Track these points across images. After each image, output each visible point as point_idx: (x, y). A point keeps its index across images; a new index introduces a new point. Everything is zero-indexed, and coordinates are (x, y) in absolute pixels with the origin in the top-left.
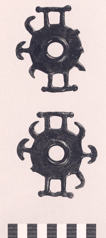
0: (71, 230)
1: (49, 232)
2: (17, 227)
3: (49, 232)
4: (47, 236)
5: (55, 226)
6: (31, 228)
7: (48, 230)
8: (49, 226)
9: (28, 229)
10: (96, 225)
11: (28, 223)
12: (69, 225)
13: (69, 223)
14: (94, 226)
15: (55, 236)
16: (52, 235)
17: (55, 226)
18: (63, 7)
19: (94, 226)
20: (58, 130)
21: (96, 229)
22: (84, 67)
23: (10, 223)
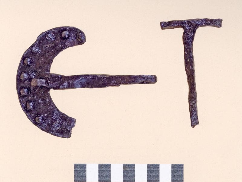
0: (177, 172)
2: (110, 167)
4: (147, 179)
5: (108, 166)
6: (103, 169)
7: (100, 171)
8: (101, 166)
9: (99, 171)
10: (183, 165)
11: (99, 163)
12: (77, 165)
13: (102, 163)
15: (157, 179)
16: (80, 177)
17: (108, 166)
18: (181, 28)
20: (50, 63)
21: (86, 170)
22: (73, 27)
23: (77, 163)
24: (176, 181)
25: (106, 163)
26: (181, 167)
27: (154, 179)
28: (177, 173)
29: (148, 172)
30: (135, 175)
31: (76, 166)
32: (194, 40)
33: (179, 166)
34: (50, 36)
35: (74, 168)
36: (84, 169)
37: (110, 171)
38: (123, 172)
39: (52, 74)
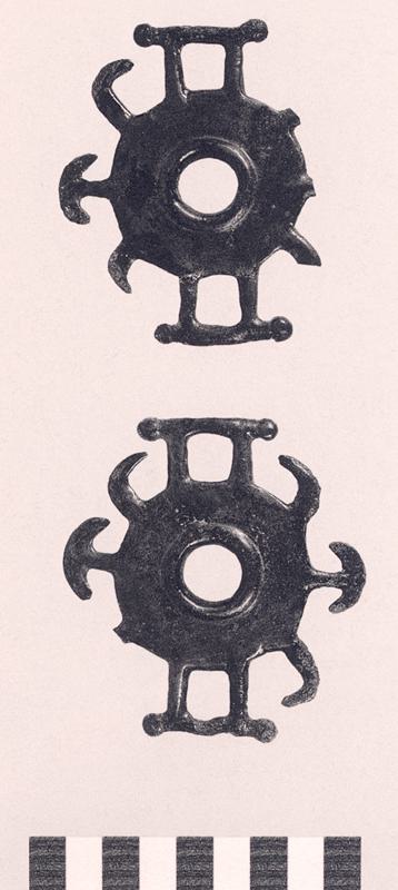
0: (266, 860)
1: (185, 867)
2: (63, 847)
3: (185, 867)
4: (175, 882)
5: (207, 844)
6: (116, 852)
7: (180, 860)
8: (183, 844)
9: (103, 858)
10: (359, 840)
11: (105, 835)
12: (260, 842)
13: (260, 835)
14: (353, 844)
15: (205, 881)
16: (194, 877)
17: (207, 844)
19: (353, 844)
20: (216, 486)
21: (359, 857)
22: (315, 251)
23: (38, 835)
26: (279, 846)
39: (85, 576)
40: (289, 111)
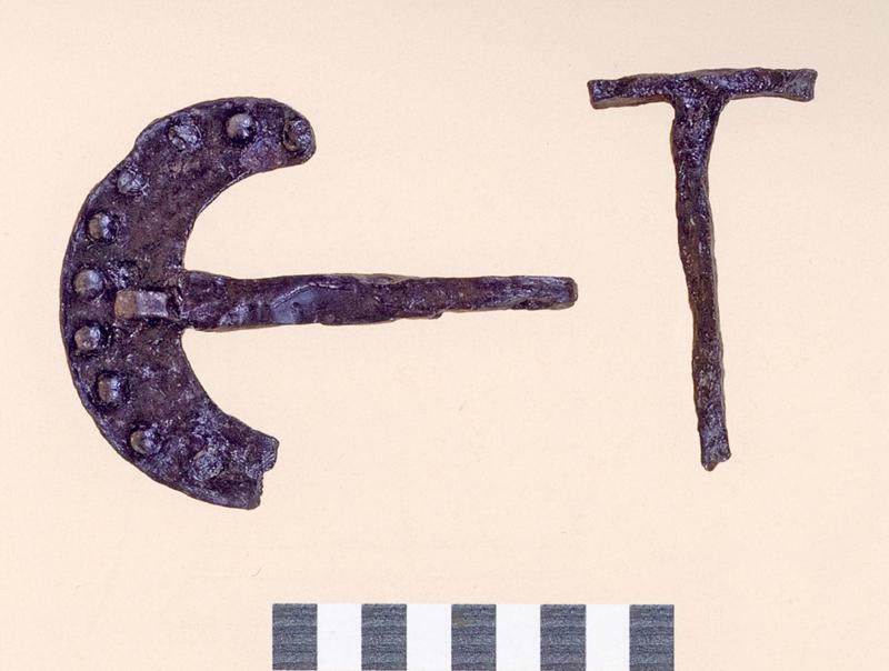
0: (649, 633)
1: (280, 659)
2: (404, 617)
3: (280, 659)
4: (539, 660)
5: (398, 612)
6: (378, 623)
7: (366, 631)
8: (369, 612)
9: (363, 629)
10: (671, 609)
11: (365, 602)
12: (284, 610)
13: (374, 603)
14: (807, 95)
15: (575, 658)
17: (398, 612)
19: (807, 95)
20: (182, 232)
21: (316, 628)
22: (269, 100)
23: (284, 602)
24: (646, 666)
25: (389, 602)
26: (663, 616)
27: (565, 659)
28: (651, 638)
29: (543, 636)
30: (494, 646)
31: (280, 612)
32: (714, 146)
33: (659, 610)
34: (183, 131)
35: (271, 619)
36: (308, 625)
37: (403, 631)
38: (453, 635)
40: (277, 443)
